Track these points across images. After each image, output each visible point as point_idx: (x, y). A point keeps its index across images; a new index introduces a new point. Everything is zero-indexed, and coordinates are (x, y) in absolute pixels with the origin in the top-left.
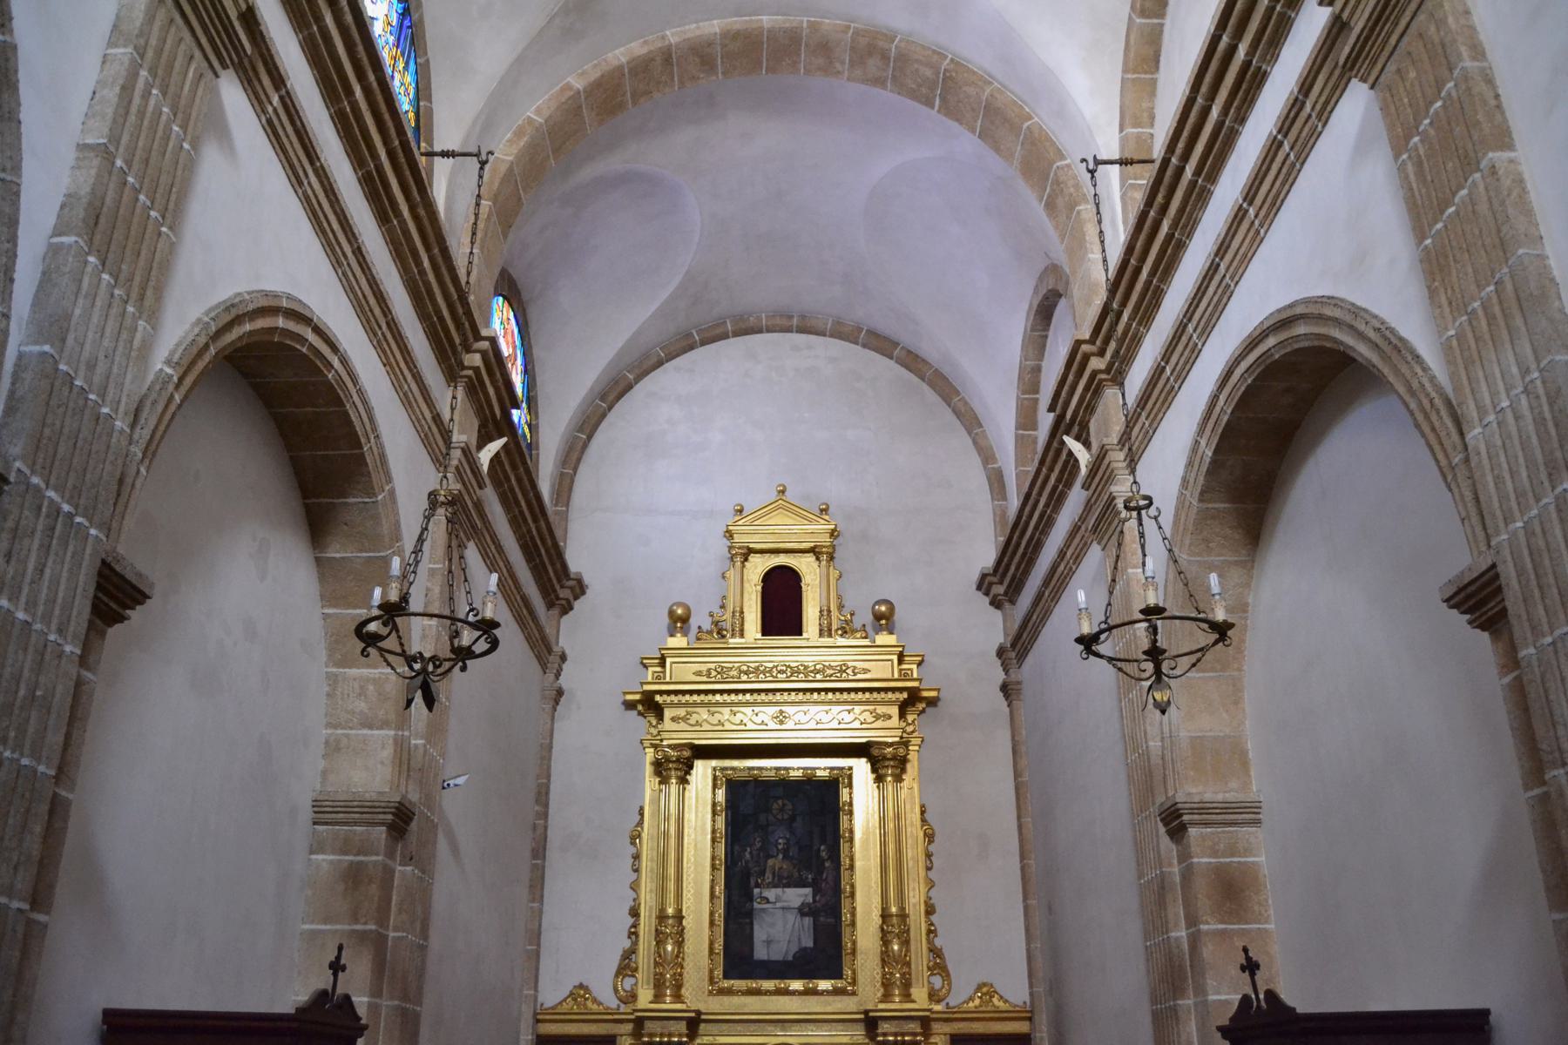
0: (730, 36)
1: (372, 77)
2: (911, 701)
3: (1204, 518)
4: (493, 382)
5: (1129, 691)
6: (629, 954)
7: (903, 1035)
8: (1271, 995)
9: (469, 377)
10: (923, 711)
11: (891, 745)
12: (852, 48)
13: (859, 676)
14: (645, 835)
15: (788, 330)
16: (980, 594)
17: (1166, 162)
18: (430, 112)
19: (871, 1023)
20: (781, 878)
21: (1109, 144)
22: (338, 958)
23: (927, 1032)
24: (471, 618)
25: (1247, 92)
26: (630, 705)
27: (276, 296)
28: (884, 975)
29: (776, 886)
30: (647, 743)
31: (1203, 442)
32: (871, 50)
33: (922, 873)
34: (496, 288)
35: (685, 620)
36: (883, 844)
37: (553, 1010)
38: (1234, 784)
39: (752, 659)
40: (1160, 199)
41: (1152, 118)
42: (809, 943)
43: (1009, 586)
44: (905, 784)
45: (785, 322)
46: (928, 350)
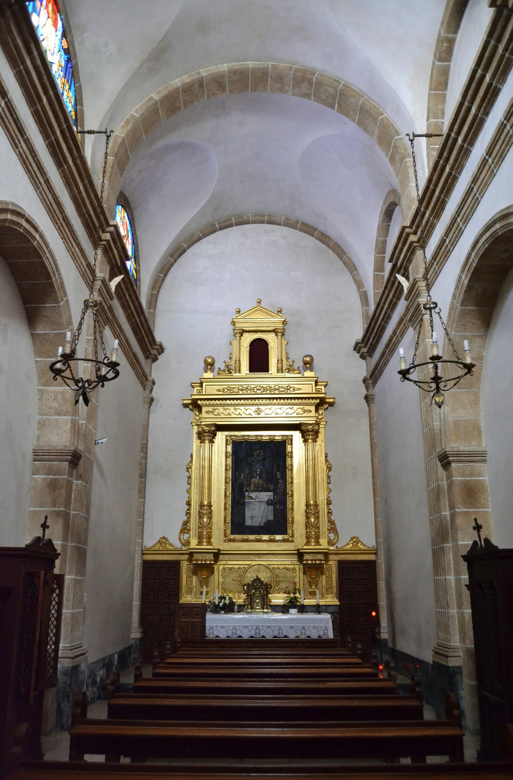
0: (233, 72)
1: (51, 93)
2: (321, 403)
3: (463, 314)
4: (116, 248)
5: (425, 398)
6: (186, 523)
7: (315, 560)
8: (487, 541)
9: (104, 245)
10: (327, 409)
11: (311, 424)
12: (294, 78)
13: (296, 392)
14: (193, 467)
15: (262, 222)
16: (355, 352)
17: (449, 135)
18: (82, 112)
19: (300, 555)
20: (258, 487)
21: (422, 128)
22: (45, 522)
23: (327, 559)
24: (106, 361)
25: (490, 99)
26: (186, 406)
27: (6, 203)
28: (307, 533)
29: (256, 491)
30: (194, 424)
31: (463, 277)
32: (303, 79)
33: (325, 485)
34: (117, 201)
35: (212, 365)
36: (307, 472)
37: (150, 549)
38: (474, 443)
39: (245, 384)
40: (445, 154)
41: (443, 114)
42: (271, 518)
43: (369, 348)
44: (318, 443)
45: (261, 219)
46: (331, 233)
